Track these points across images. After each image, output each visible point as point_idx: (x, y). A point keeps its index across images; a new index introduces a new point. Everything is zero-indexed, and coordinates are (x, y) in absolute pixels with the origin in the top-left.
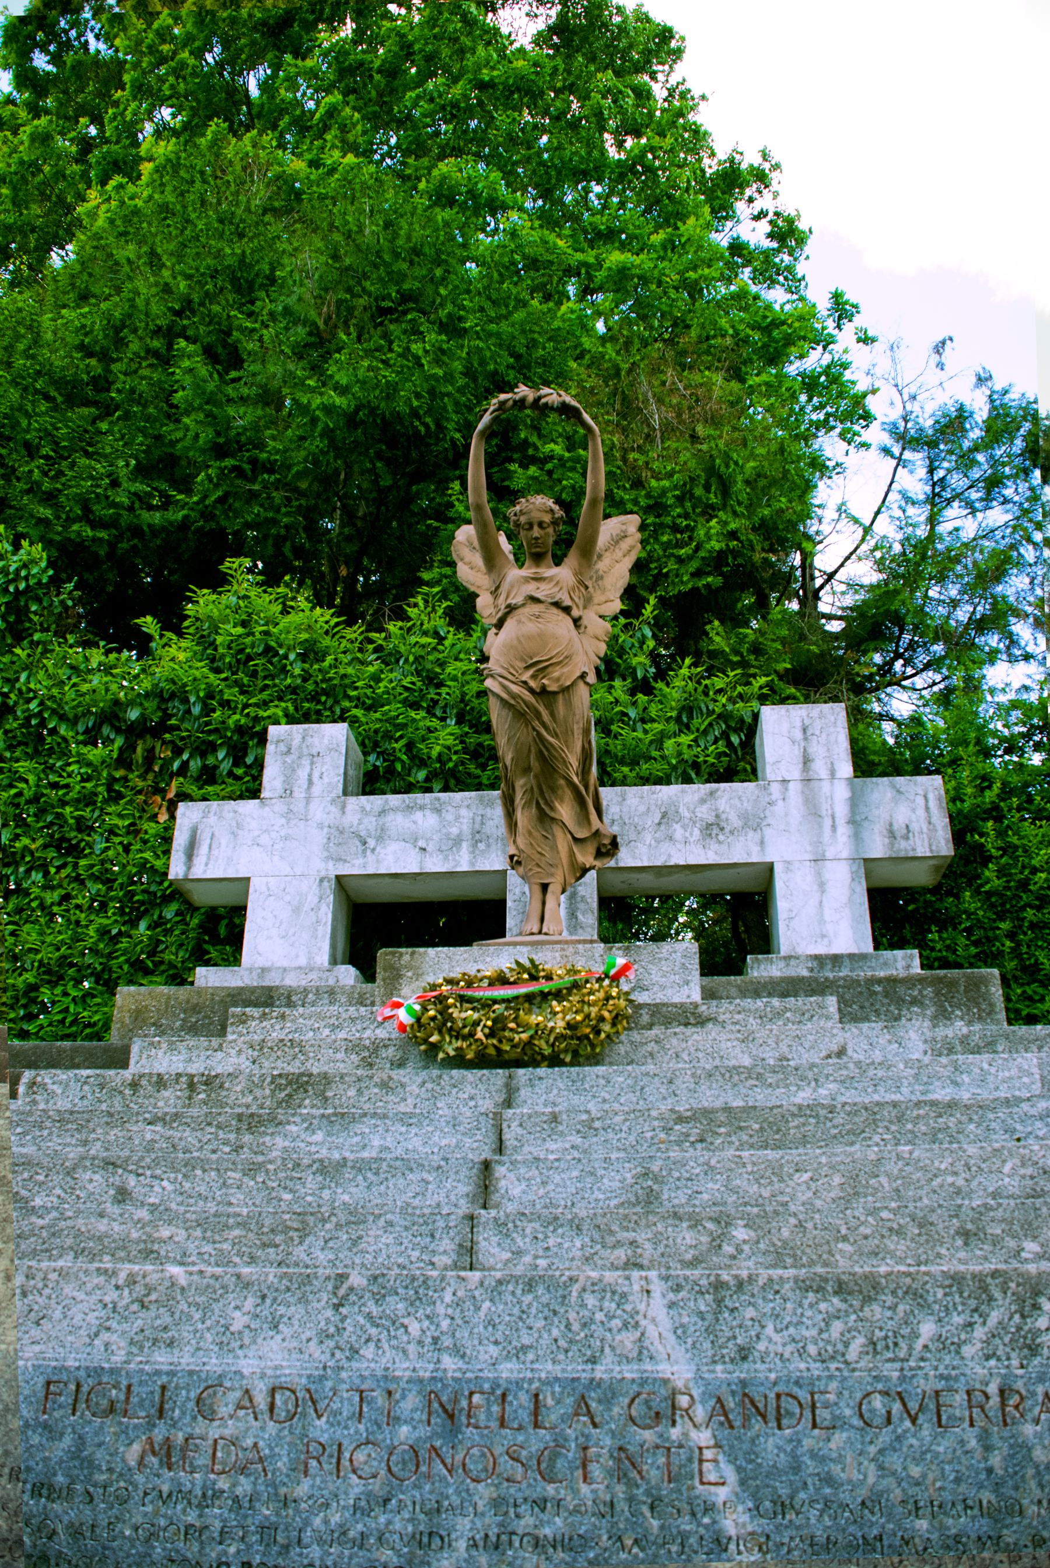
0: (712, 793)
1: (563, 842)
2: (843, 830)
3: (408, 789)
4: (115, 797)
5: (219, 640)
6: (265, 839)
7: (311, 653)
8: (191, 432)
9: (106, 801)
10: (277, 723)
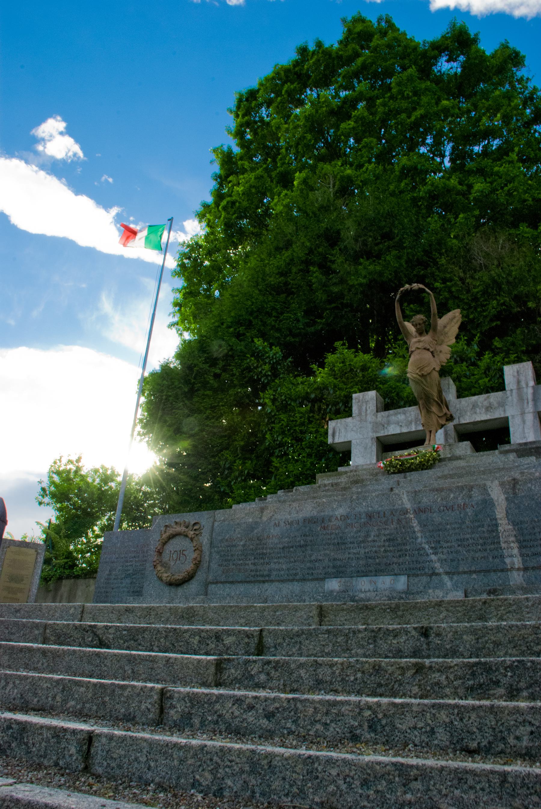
0: (488, 397)
1: (434, 418)
2: (531, 403)
3: (400, 407)
4: (310, 422)
5: (336, 369)
6: (355, 429)
7: (364, 368)
8: (320, 296)
9: (308, 424)
10: (356, 393)
